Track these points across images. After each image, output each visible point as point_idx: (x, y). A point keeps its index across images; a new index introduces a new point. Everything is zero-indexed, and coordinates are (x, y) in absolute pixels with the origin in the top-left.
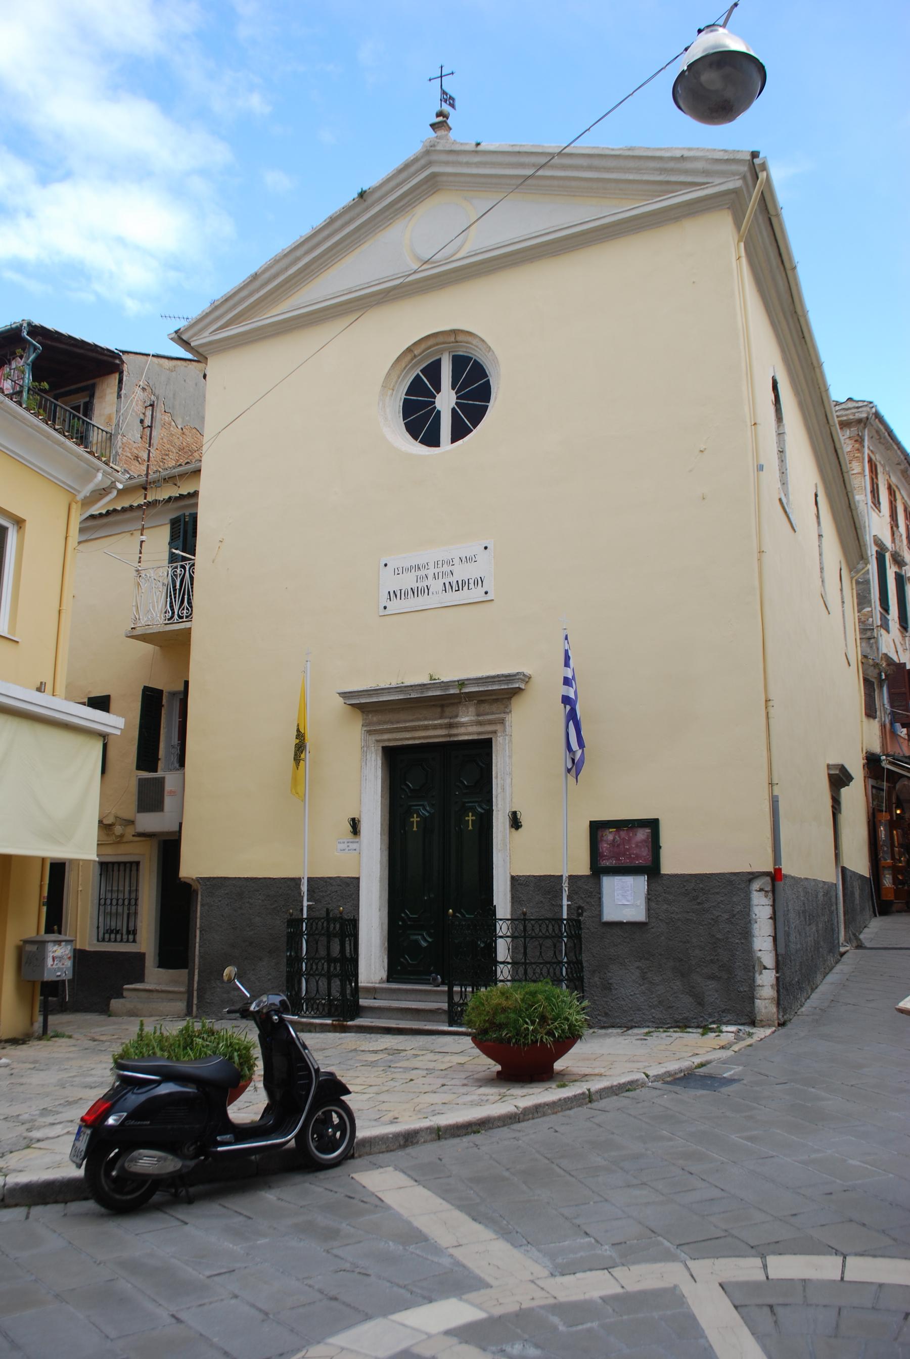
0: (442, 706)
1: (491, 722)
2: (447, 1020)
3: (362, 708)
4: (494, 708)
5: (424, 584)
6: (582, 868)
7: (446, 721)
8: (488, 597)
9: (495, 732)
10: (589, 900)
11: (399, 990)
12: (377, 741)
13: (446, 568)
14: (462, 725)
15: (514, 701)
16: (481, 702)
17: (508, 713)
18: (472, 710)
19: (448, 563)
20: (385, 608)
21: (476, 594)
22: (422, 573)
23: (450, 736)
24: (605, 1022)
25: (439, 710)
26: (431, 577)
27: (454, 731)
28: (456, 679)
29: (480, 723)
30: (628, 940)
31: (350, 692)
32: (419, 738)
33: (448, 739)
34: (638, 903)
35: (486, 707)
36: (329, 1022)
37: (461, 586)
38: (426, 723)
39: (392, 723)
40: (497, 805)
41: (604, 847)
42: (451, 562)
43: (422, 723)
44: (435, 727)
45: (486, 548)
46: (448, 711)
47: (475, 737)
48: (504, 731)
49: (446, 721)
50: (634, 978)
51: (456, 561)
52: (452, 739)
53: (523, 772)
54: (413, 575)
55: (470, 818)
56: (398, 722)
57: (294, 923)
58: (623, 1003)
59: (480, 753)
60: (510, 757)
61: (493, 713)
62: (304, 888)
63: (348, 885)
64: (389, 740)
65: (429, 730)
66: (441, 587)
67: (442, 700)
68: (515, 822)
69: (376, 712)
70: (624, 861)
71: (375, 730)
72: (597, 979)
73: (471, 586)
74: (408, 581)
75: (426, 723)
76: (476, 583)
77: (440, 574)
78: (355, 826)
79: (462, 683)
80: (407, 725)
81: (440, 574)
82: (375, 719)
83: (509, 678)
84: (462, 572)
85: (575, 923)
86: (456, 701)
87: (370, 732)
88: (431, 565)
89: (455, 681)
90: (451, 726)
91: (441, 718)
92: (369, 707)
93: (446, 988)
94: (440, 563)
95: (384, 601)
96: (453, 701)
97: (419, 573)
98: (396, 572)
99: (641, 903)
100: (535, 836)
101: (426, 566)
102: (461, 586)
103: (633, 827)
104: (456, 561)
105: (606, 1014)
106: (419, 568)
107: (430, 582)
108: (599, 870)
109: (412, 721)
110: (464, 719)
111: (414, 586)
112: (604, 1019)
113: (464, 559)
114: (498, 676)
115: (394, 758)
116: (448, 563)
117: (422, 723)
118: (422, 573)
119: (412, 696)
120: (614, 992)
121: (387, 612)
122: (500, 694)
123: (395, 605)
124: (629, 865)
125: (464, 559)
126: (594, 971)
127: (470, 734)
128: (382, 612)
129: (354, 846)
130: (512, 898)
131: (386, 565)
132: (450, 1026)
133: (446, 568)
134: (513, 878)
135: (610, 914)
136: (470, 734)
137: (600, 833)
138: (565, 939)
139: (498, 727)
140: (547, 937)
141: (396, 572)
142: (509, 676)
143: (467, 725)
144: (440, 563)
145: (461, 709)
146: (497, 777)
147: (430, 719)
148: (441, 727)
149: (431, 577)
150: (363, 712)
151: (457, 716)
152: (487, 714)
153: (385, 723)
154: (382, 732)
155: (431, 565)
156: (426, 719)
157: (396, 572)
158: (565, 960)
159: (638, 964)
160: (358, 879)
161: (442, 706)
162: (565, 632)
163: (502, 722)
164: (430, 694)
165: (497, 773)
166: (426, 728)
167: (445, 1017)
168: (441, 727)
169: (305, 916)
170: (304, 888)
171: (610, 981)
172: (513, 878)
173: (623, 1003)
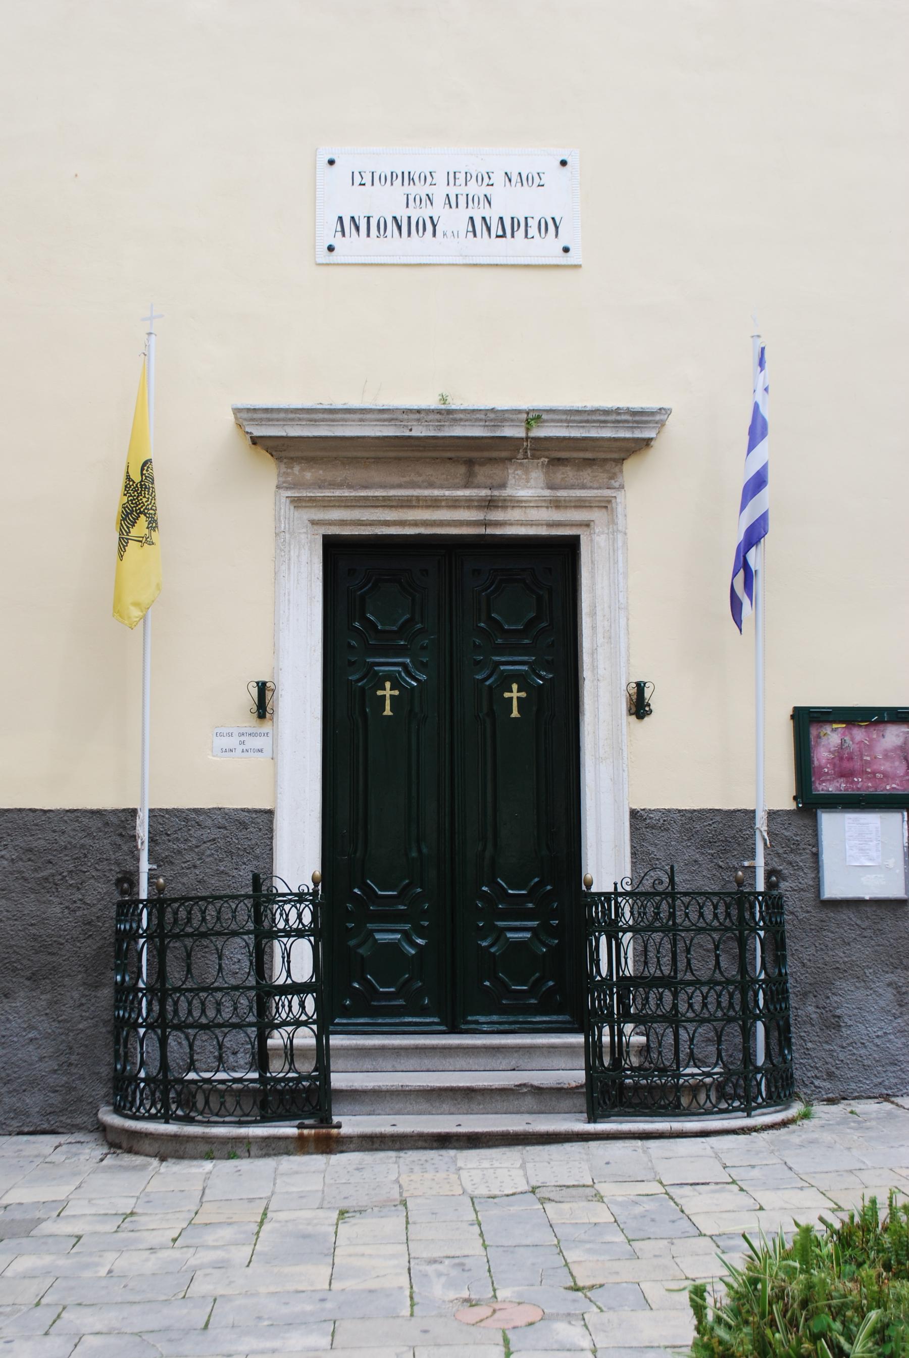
0: (470, 463)
1: (581, 504)
2: (585, 1108)
3: (279, 449)
4: (586, 475)
5: (426, 212)
6: (783, 798)
7: (484, 493)
8: (570, 259)
9: (587, 525)
10: (792, 857)
11: (383, 1049)
12: (313, 523)
13: (473, 188)
14: (516, 503)
15: (628, 466)
16: (557, 462)
17: (622, 487)
18: (537, 476)
19: (480, 179)
20: (331, 249)
21: (545, 249)
22: (420, 189)
23: (486, 524)
24: (828, 1091)
25: (462, 470)
26: (439, 200)
27: (497, 515)
28: (524, 406)
29: (557, 504)
30: (868, 933)
31: (266, 410)
32: (415, 524)
33: (481, 531)
34: (891, 863)
35: (567, 473)
36: (292, 1131)
37: (508, 228)
38: (436, 492)
39: (350, 487)
40: (594, 668)
41: (822, 755)
42: (486, 179)
43: (427, 492)
44: (454, 504)
45: (564, 163)
46: (482, 473)
47: (543, 531)
48: (612, 521)
49: (484, 493)
50: (882, 1003)
51: (498, 178)
52: (490, 531)
53: (635, 611)
54: (398, 191)
55: (515, 694)
56: (365, 487)
57: (127, 907)
58: (863, 1051)
59: (556, 561)
60: (626, 575)
61: (583, 487)
62: (143, 830)
63: (243, 825)
64: (343, 523)
65: (442, 511)
66: (465, 224)
67: (475, 451)
68: (639, 706)
69: (311, 461)
70: (862, 785)
71: (312, 499)
72: (811, 1009)
73: (533, 231)
74: (388, 202)
75: (436, 492)
76: (542, 227)
77: (462, 201)
78: (263, 703)
79: (534, 417)
80: (392, 493)
81: (462, 201)
82: (308, 475)
83: (639, 417)
84: (508, 202)
85: (774, 902)
86: (504, 454)
87: (297, 502)
88: (440, 178)
89: (519, 411)
90: (490, 504)
91: (466, 486)
92: (293, 448)
93: (579, 1039)
94: (461, 177)
95: (327, 233)
96: (495, 454)
97: (412, 190)
98: (358, 179)
99: (896, 862)
100: (669, 737)
101: (428, 177)
102: (508, 228)
103: (881, 722)
104: (498, 178)
105: (830, 1075)
106: (411, 180)
107: (438, 210)
108: (811, 802)
109: (400, 486)
110: (523, 493)
111: (402, 214)
112: (826, 1084)
113: (515, 178)
114: (618, 411)
115: (343, 559)
116: (480, 179)
117: (427, 492)
118: (420, 189)
119: (414, 433)
120: (845, 1032)
121: (334, 258)
122: (602, 450)
123: (353, 247)
124: (871, 791)
125: (515, 178)
126: (805, 994)
127: (531, 524)
128: (323, 256)
129: (257, 742)
130: (634, 854)
131: (331, 162)
132: (592, 1119)
133: (473, 188)
134: (634, 814)
135: (837, 884)
136: (531, 524)
137: (813, 731)
138: (762, 933)
139: (595, 515)
140: (700, 930)
141: (358, 180)
142: (642, 413)
143: (527, 507)
144: (461, 177)
145: (513, 474)
146: (593, 614)
147: (441, 487)
148: (468, 503)
149: (439, 200)
150: (279, 459)
151: (503, 486)
152: (572, 487)
153: (333, 485)
154: (313, 502)
155: (440, 178)
156: (431, 485)
157: (358, 180)
158: (762, 977)
159: (890, 977)
160: (270, 813)
161: (470, 463)
162: (760, 343)
163: (606, 505)
164: (459, 431)
165: (594, 607)
166: (434, 503)
167: (582, 1102)
168: (468, 503)
169: (144, 895)
170: (143, 830)
171: (838, 1012)
172: (634, 814)
173: (863, 1051)
